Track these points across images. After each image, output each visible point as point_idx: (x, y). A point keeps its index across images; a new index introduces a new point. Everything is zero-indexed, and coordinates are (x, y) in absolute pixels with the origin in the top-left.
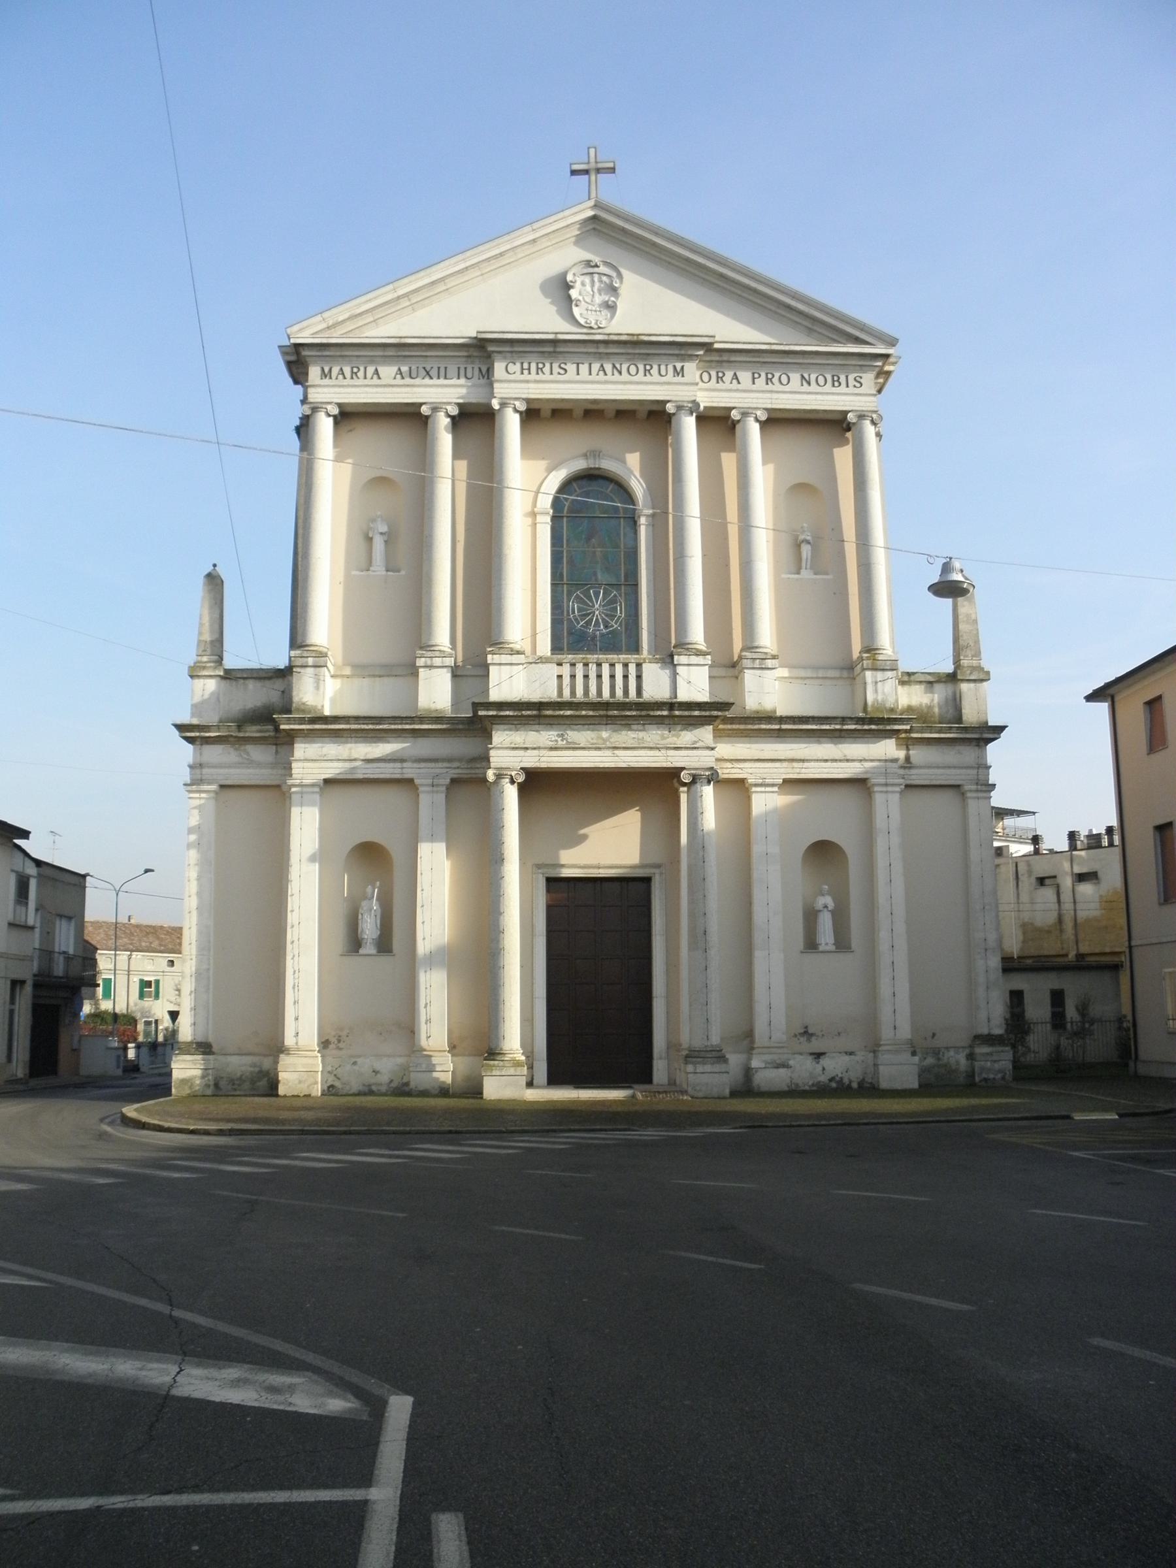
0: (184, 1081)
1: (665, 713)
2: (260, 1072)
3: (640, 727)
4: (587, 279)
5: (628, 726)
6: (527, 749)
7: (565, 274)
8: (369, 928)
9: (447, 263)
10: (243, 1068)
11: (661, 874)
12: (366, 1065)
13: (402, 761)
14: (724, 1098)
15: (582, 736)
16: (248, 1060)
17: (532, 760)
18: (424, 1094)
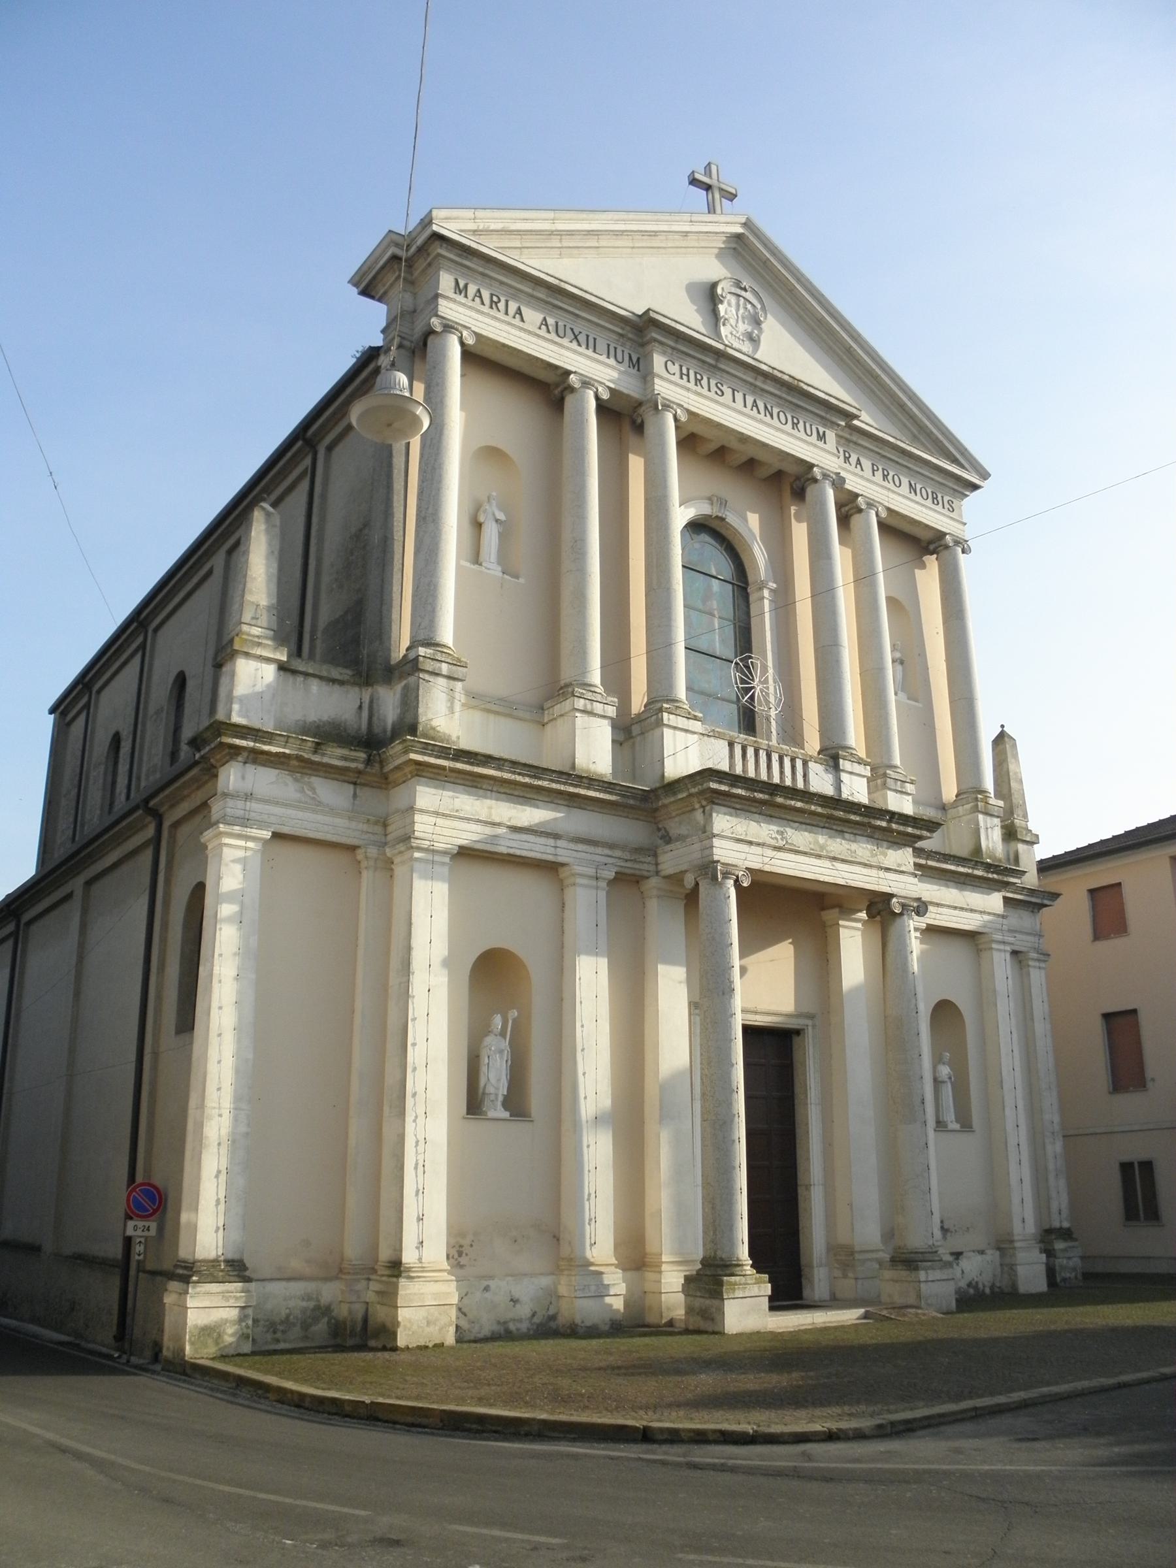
0: (207, 1331)
1: (884, 824)
4: (733, 300)
6: (750, 843)
7: (714, 286)
8: (495, 1077)
9: (610, 215)
10: (291, 1304)
11: (814, 1026)
12: (502, 1288)
13: (556, 836)
15: (801, 837)
16: (298, 1288)
17: (756, 859)
18: (592, 1332)
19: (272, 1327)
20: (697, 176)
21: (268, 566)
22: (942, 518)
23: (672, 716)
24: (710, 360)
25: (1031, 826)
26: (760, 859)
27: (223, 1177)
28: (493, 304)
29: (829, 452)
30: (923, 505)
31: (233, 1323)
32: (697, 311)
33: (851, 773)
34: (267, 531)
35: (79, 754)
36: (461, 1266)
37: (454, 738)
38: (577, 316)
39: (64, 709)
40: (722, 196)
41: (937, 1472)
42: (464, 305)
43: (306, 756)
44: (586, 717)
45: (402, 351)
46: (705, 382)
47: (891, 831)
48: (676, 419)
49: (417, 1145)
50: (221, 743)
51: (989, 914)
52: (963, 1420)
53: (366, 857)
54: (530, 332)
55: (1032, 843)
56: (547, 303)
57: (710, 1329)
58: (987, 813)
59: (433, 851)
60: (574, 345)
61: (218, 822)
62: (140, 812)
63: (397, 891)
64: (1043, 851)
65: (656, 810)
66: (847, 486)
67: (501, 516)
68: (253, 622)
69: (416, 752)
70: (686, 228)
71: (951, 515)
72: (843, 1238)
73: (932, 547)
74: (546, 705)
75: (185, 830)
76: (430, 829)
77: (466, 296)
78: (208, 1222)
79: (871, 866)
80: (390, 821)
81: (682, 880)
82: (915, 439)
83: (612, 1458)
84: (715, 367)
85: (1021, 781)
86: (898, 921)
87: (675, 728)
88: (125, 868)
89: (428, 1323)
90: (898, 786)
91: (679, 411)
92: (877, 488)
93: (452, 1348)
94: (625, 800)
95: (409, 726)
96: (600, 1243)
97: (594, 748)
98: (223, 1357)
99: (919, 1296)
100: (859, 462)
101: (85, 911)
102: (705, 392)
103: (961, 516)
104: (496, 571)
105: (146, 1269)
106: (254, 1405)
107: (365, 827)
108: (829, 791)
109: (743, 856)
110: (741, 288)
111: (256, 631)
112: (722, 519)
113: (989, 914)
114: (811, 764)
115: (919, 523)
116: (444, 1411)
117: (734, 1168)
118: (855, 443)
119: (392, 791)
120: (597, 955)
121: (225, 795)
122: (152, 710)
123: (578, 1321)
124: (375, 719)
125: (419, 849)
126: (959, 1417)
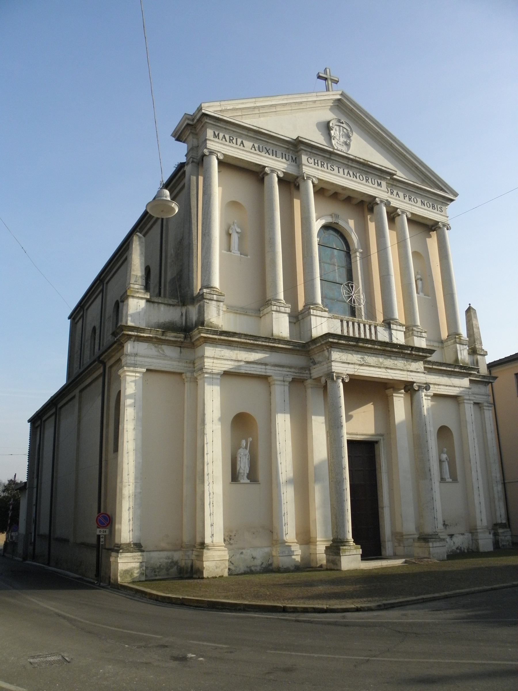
1: (409, 352)
2: (172, 562)
3: (395, 358)
4: (337, 128)
5: (390, 357)
6: (349, 363)
7: (329, 122)
8: (244, 466)
9: (280, 97)
10: (161, 560)
11: (383, 439)
12: (248, 553)
13: (266, 364)
14: (445, 560)
15: (371, 360)
17: (351, 370)
18: (287, 570)
19: (154, 570)
20: (321, 75)
21: (141, 259)
22: (437, 215)
23: (314, 311)
24: (328, 156)
25: (483, 348)
26: (353, 370)
27: (131, 510)
28: (231, 141)
29: (383, 191)
30: (428, 210)
31: (137, 569)
32: (321, 134)
33: (396, 330)
34: (140, 244)
35: (80, 335)
36: (231, 544)
37: (220, 326)
38: (268, 142)
39: (73, 317)
40: (332, 82)
41: (394, 623)
42: (218, 142)
43: (159, 337)
44: (277, 314)
45: (194, 164)
46: (325, 165)
47: (413, 355)
48: (313, 183)
49: (210, 495)
50: (123, 334)
51: (463, 387)
52: (418, 603)
53: (186, 377)
54: (247, 151)
55: (484, 355)
56: (254, 138)
57: (336, 569)
58: (460, 344)
59: (213, 373)
60: (267, 155)
61: (124, 366)
62: (97, 362)
63: (199, 391)
64: (490, 359)
65: (309, 351)
66: (391, 205)
67: (239, 230)
68: (135, 283)
69: (204, 333)
70: (315, 99)
71: (441, 213)
72: (398, 529)
73: (433, 228)
74: (261, 309)
75: (114, 369)
76: (211, 364)
77: (219, 139)
78: (126, 530)
79: (404, 370)
80: (196, 361)
81: (320, 380)
82: (423, 182)
83: (267, 618)
84: (330, 158)
85: (478, 328)
86: (417, 393)
87: (316, 316)
88: (93, 385)
89: (217, 568)
90: (419, 334)
91: (314, 179)
92: (406, 205)
93: (226, 577)
94: (295, 348)
95: (201, 322)
96: (290, 533)
97: (281, 326)
98: (133, 582)
99: (429, 554)
100: (397, 194)
101: (80, 403)
102: (326, 170)
103: (446, 213)
104: (238, 254)
105: (105, 547)
106: (140, 600)
107: (185, 365)
108: (387, 340)
109: (345, 369)
110: (341, 123)
111: (136, 286)
112: (337, 224)
113: (463, 387)
114: (378, 328)
115: (426, 218)
116: (208, 601)
117: (344, 501)
118: (396, 186)
119: (196, 350)
120: (285, 413)
121: (127, 355)
122: (107, 316)
123: (281, 566)
124: (188, 320)
125: (207, 373)
126: (416, 602)
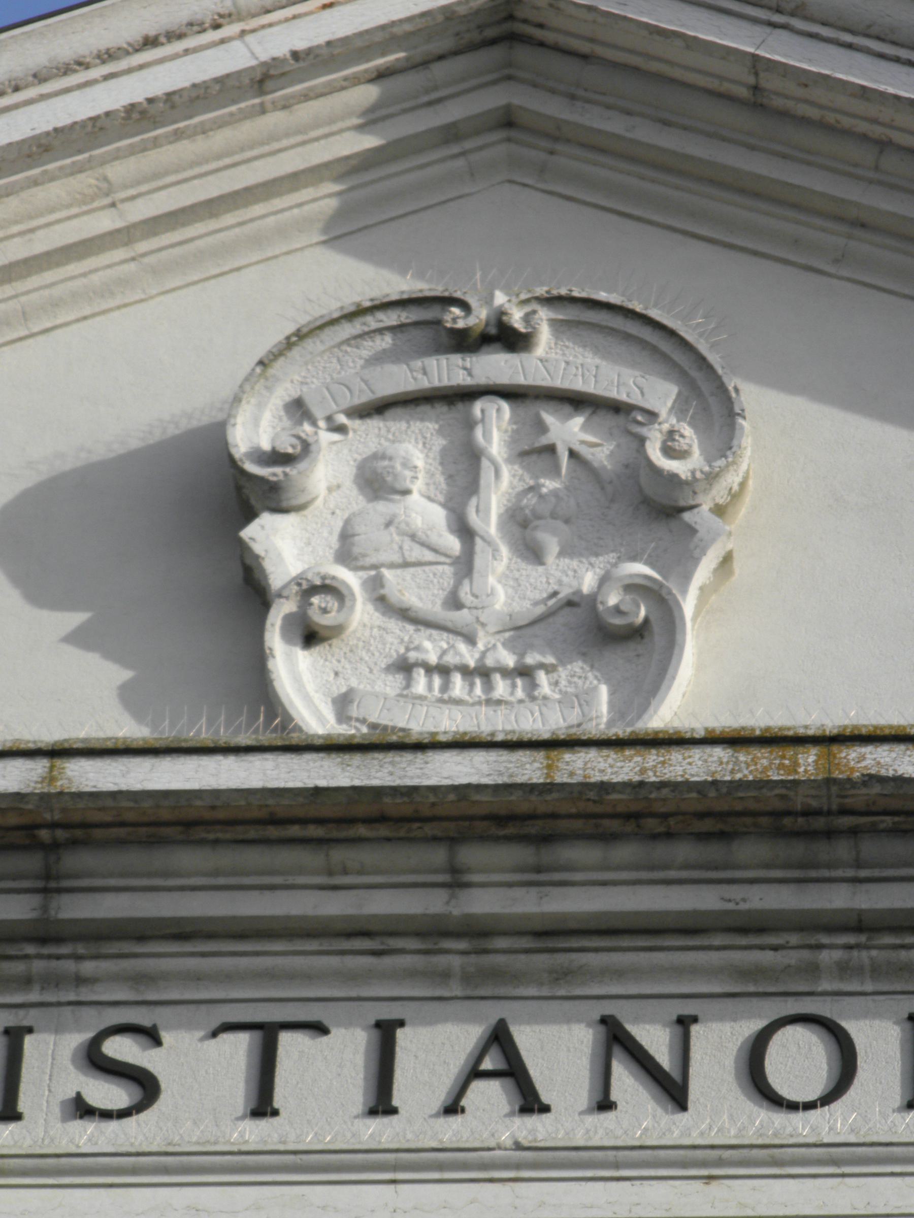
84: (46, 934)
110: (464, 342)
